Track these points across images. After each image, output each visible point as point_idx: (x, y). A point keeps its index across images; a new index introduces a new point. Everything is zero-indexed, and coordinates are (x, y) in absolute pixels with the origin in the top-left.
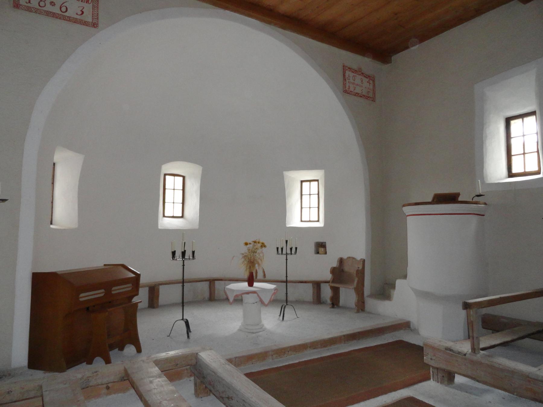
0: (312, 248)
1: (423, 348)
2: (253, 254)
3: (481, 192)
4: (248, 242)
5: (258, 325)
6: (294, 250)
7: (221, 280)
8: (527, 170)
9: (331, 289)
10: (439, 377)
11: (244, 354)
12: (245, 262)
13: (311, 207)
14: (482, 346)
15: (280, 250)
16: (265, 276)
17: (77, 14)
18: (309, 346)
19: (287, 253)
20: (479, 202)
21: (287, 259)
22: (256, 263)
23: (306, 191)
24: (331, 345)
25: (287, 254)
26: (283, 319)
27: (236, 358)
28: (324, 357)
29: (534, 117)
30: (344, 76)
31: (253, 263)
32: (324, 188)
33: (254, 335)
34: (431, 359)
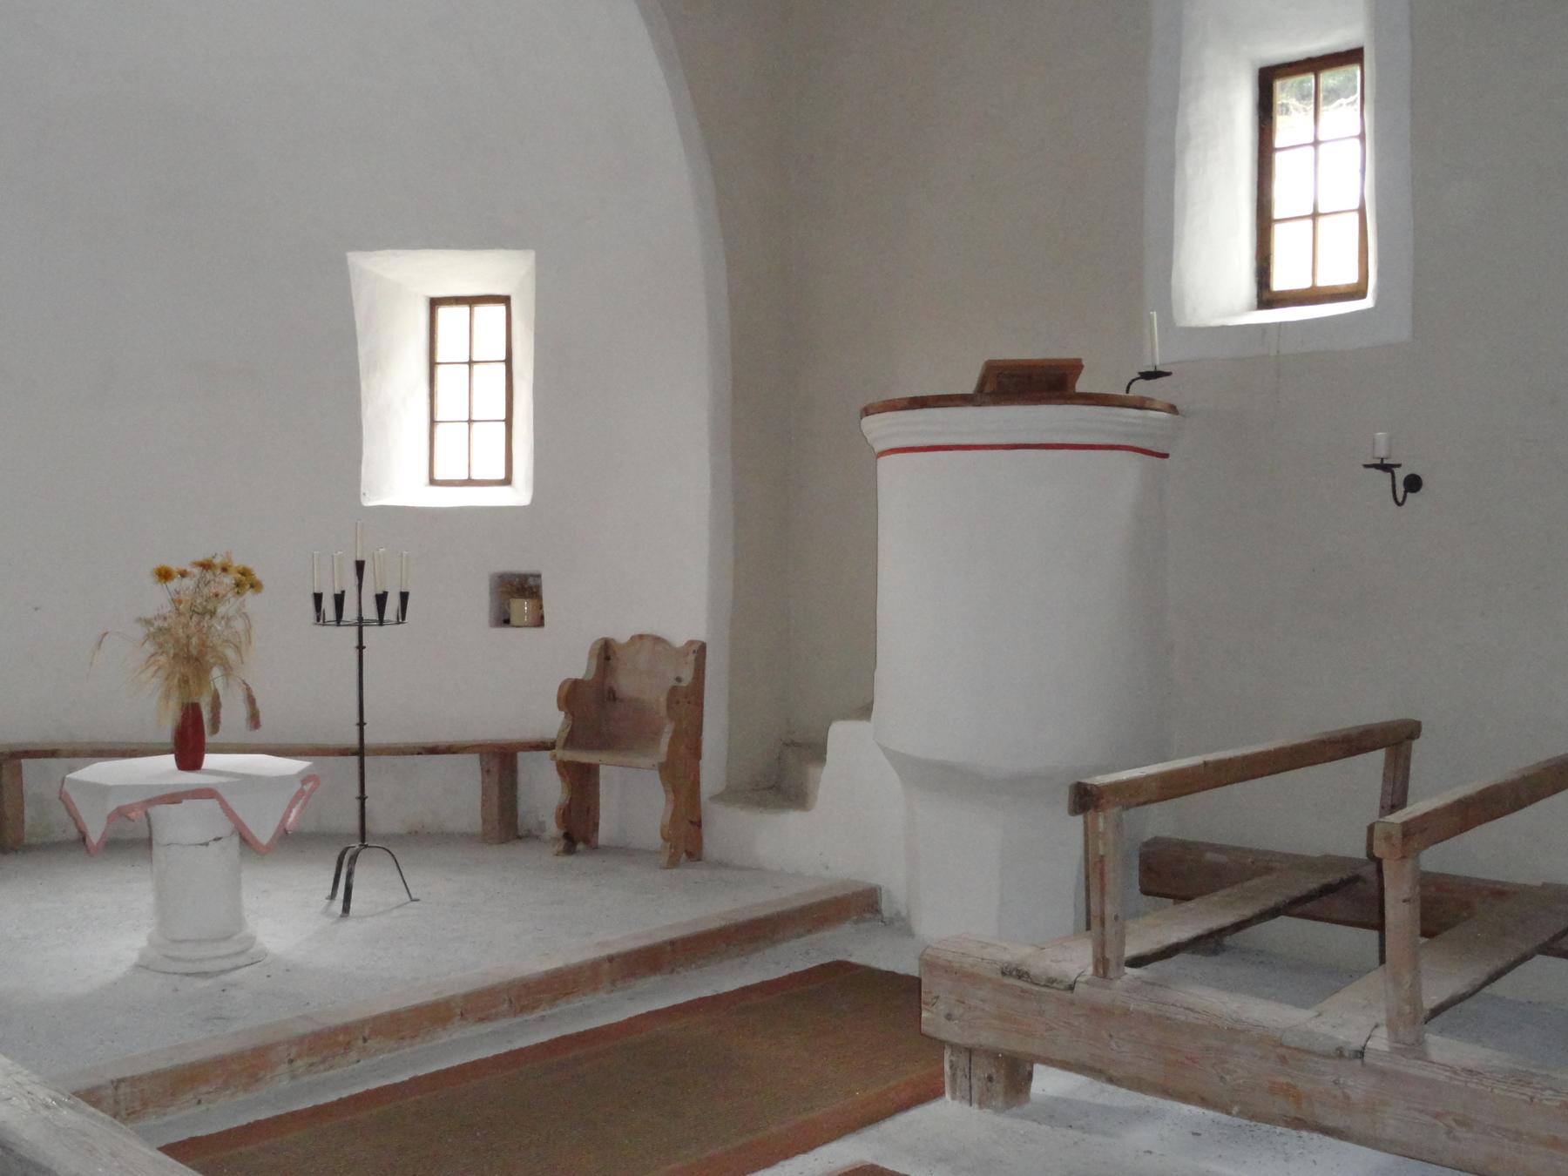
0: (481, 602)
1: (918, 981)
2: (198, 623)
3: (1158, 363)
4: (174, 565)
5: (227, 938)
6: (393, 604)
7: (53, 753)
8: (1321, 283)
9: (561, 774)
10: (974, 1081)
11: (162, 1065)
12: (163, 659)
13: (474, 418)
14: (1131, 950)
15: (328, 605)
16: (254, 720)
18: (458, 1011)
19: (360, 619)
20: (1152, 400)
21: (361, 647)
22: (214, 664)
23: (451, 345)
24: (553, 1002)
25: (361, 623)
26: (346, 909)
27: (117, 1083)
28: (521, 1051)
29: (1356, 70)
31: (197, 659)
32: (532, 334)
33: (209, 983)
34: (949, 1017)
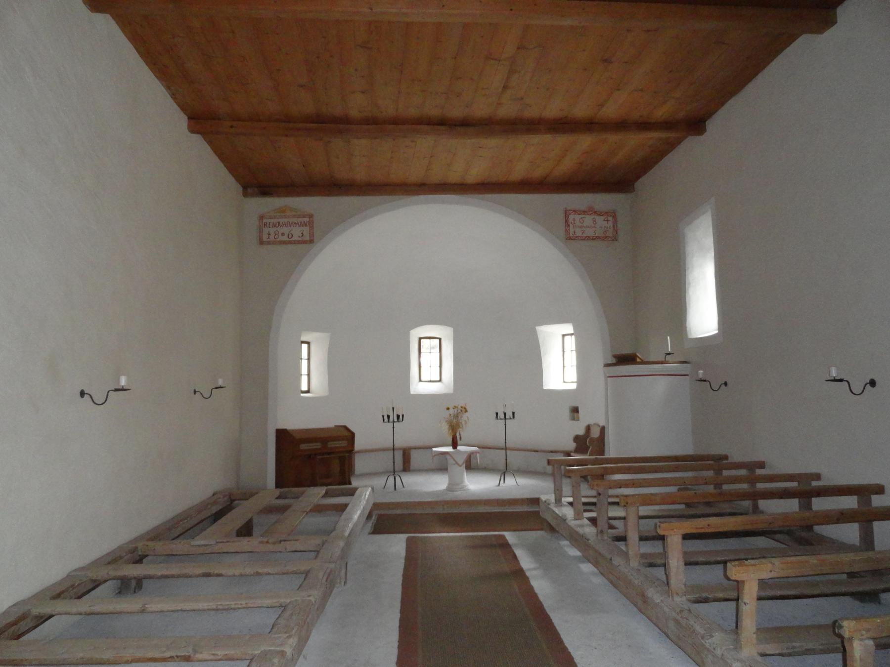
6: (401, 417)
17: (299, 237)
25: (394, 422)
30: (567, 221)
